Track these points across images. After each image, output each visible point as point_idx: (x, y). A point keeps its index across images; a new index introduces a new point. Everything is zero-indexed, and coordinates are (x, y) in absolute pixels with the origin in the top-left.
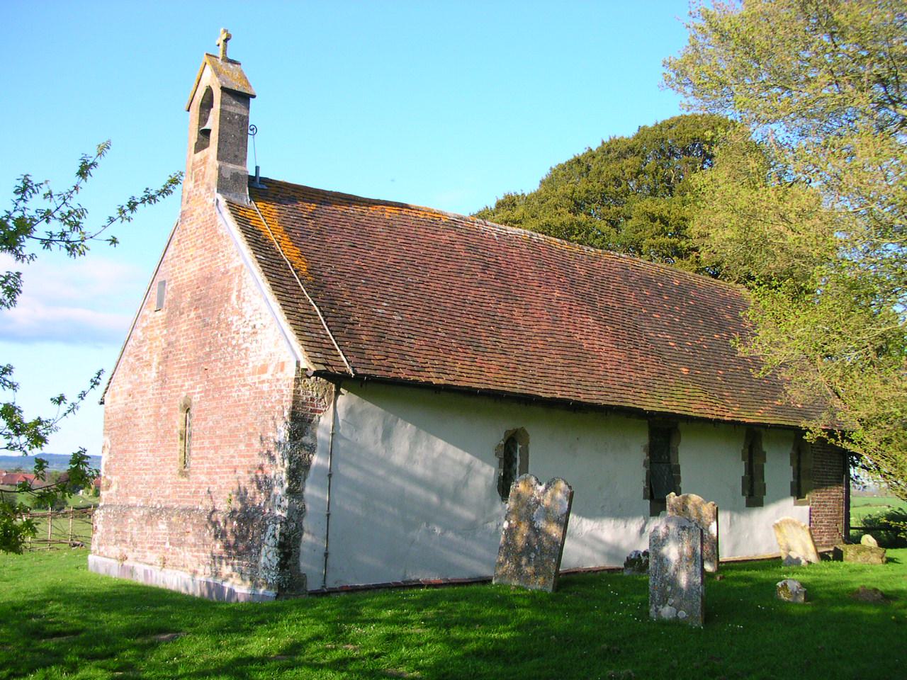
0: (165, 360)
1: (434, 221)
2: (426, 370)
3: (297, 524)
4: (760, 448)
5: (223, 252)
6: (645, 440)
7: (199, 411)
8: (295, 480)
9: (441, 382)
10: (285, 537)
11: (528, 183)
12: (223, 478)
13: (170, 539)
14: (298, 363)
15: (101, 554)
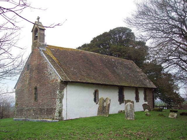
0: (30, 79)
1: (72, 50)
4: (138, 91)
6: (118, 91)
14: (61, 79)
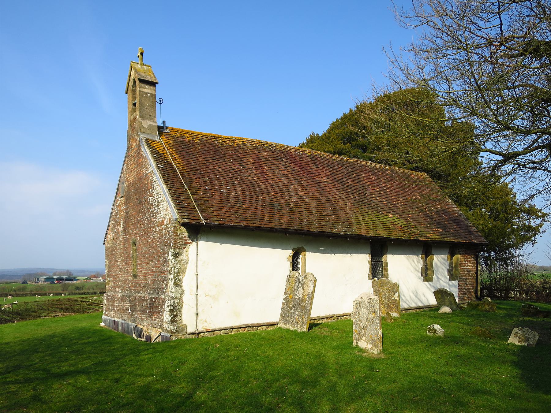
2: (247, 219)
3: (180, 300)
5: (144, 165)
7: (139, 245)
8: (178, 278)
9: (255, 225)
10: (173, 307)
11: (321, 129)
12: (150, 278)
13: (130, 308)
15: (106, 315)
